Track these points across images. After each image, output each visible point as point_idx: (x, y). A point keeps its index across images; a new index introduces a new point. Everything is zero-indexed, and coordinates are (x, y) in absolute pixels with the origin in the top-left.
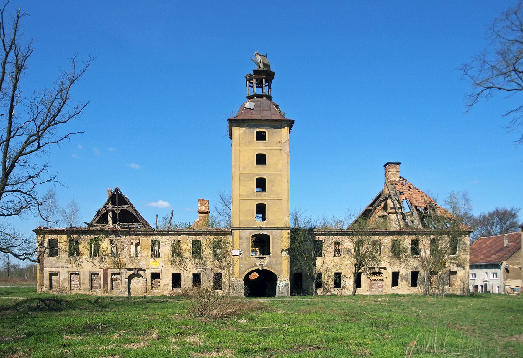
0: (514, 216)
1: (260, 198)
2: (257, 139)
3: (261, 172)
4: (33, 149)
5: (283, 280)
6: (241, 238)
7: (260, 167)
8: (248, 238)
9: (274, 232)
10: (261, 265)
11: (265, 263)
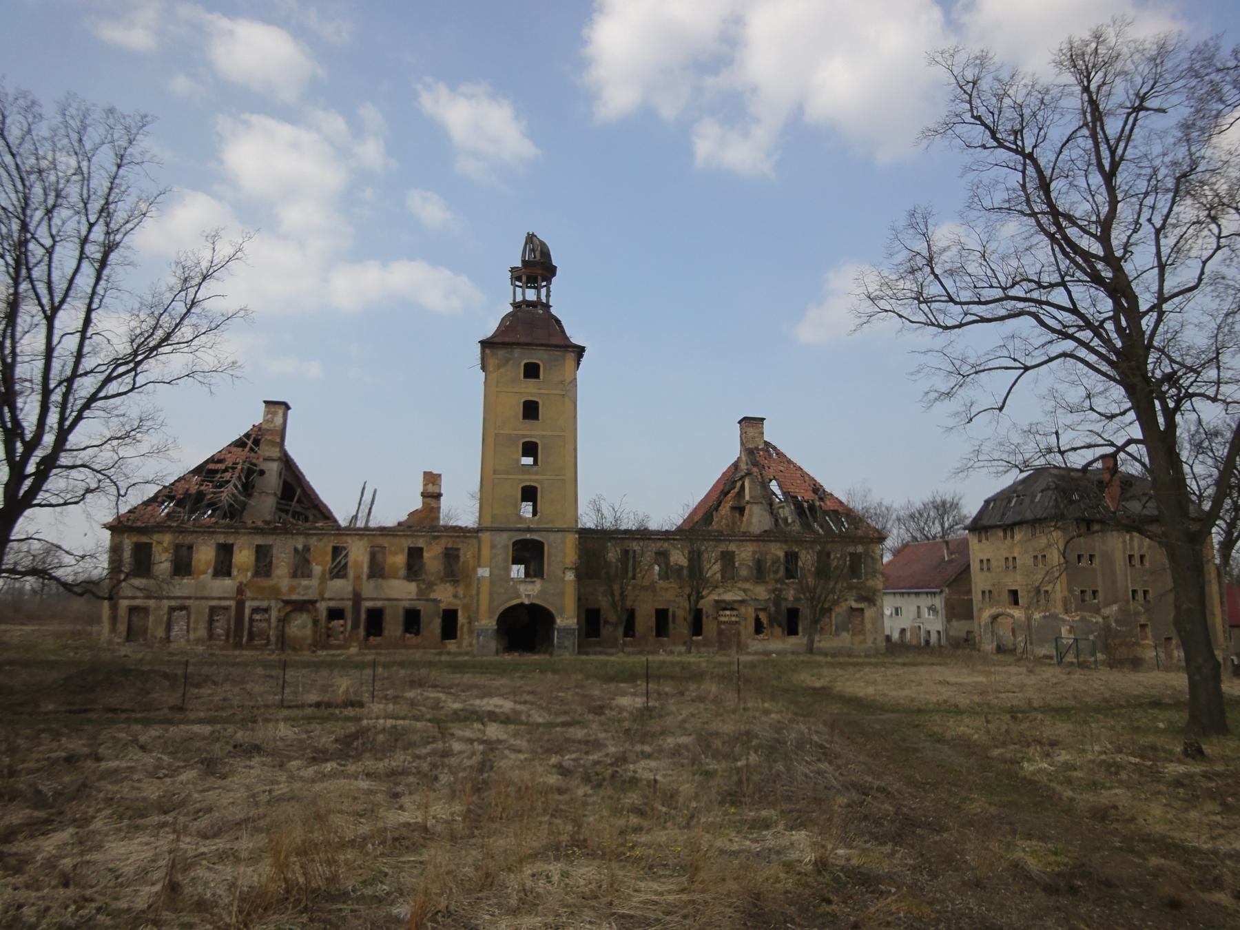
0: (955, 506)
1: (526, 477)
2: (526, 376)
3: (532, 431)
4: (123, 389)
5: (567, 619)
6: (493, 546)
7: (530, 423)
8: (506, 547)
9: (552, 536)
10: (528, 596)
11: (530, 592)
